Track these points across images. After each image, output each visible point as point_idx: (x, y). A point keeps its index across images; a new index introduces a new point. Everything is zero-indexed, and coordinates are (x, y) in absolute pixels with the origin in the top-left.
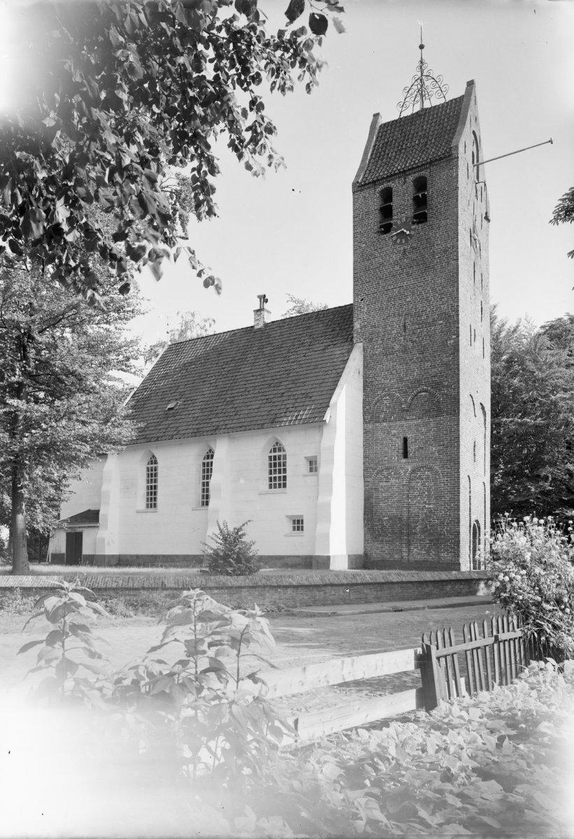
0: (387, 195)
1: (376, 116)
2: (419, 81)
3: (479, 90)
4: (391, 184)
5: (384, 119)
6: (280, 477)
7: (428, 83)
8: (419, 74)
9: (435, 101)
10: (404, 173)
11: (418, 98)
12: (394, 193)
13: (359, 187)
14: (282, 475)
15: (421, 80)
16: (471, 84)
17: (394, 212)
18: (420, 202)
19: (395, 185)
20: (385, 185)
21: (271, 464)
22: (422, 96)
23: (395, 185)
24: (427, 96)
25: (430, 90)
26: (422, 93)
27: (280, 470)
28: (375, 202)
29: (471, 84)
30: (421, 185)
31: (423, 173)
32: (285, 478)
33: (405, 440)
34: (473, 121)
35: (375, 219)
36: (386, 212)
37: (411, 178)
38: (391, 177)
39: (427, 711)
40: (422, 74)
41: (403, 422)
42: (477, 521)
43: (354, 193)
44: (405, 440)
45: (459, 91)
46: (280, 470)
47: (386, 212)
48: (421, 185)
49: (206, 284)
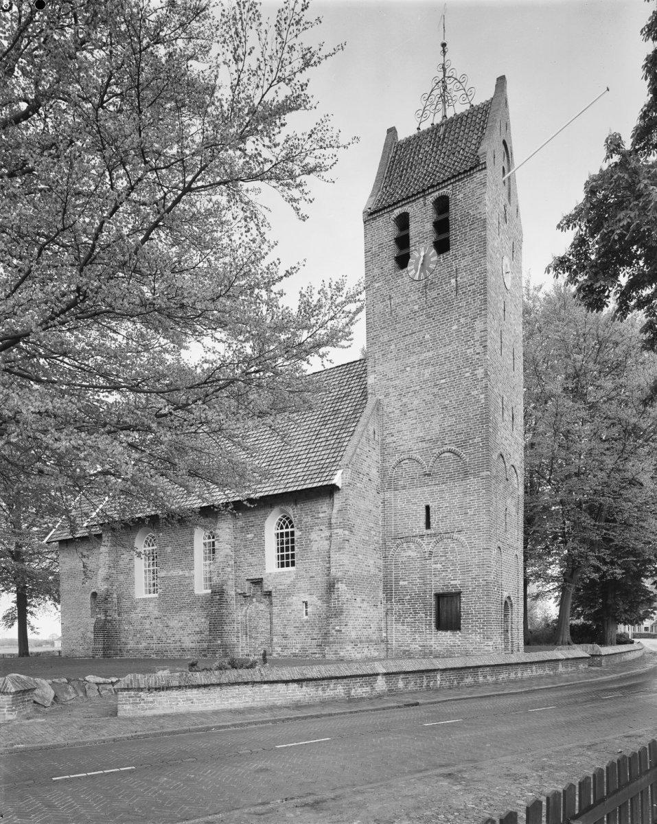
0: (403, 222)
1: (392, 131)
2: (440, 84)
3: (511, 90)
4: (406, 209)
5: (402, 136)
6: (288, 555)
7: (451, 85)
8: (441, 75)
9: (459, 108)
10: (423, 192)
11: (440, 106)
12: (412, 220)
13: (372, 215)
14: (290, 552)
15: (443, 82)
16: (501, 81)
17: (412, 242)
18: (442, 227)
19: (410, 209)
20: (397, 212)
21: (278, 556)
22: (444, 102)
23: (410, 209)
24: (450, 101)
25: (454, 93)
26: (444, 98)
27: (288, 558)
28: (387, 229)
29: (501, 81)
30: (442, 205)
31: (444, 191)
32: (293, 556)
33: (428, 508)
34: (503, 129)
35: (391, 251)
36: (403, 242)
37: (431, 199)
38: (408, 199)
39: (395, 257)
40: (444, 76)
41: (425, 489)
42: (509, 598)
43: (365, 222)
44: (428, 508)
45: (483, 94)
46: (287, 548)
47: (403, 242)
48: (442, 205)
49: (276, 244)
